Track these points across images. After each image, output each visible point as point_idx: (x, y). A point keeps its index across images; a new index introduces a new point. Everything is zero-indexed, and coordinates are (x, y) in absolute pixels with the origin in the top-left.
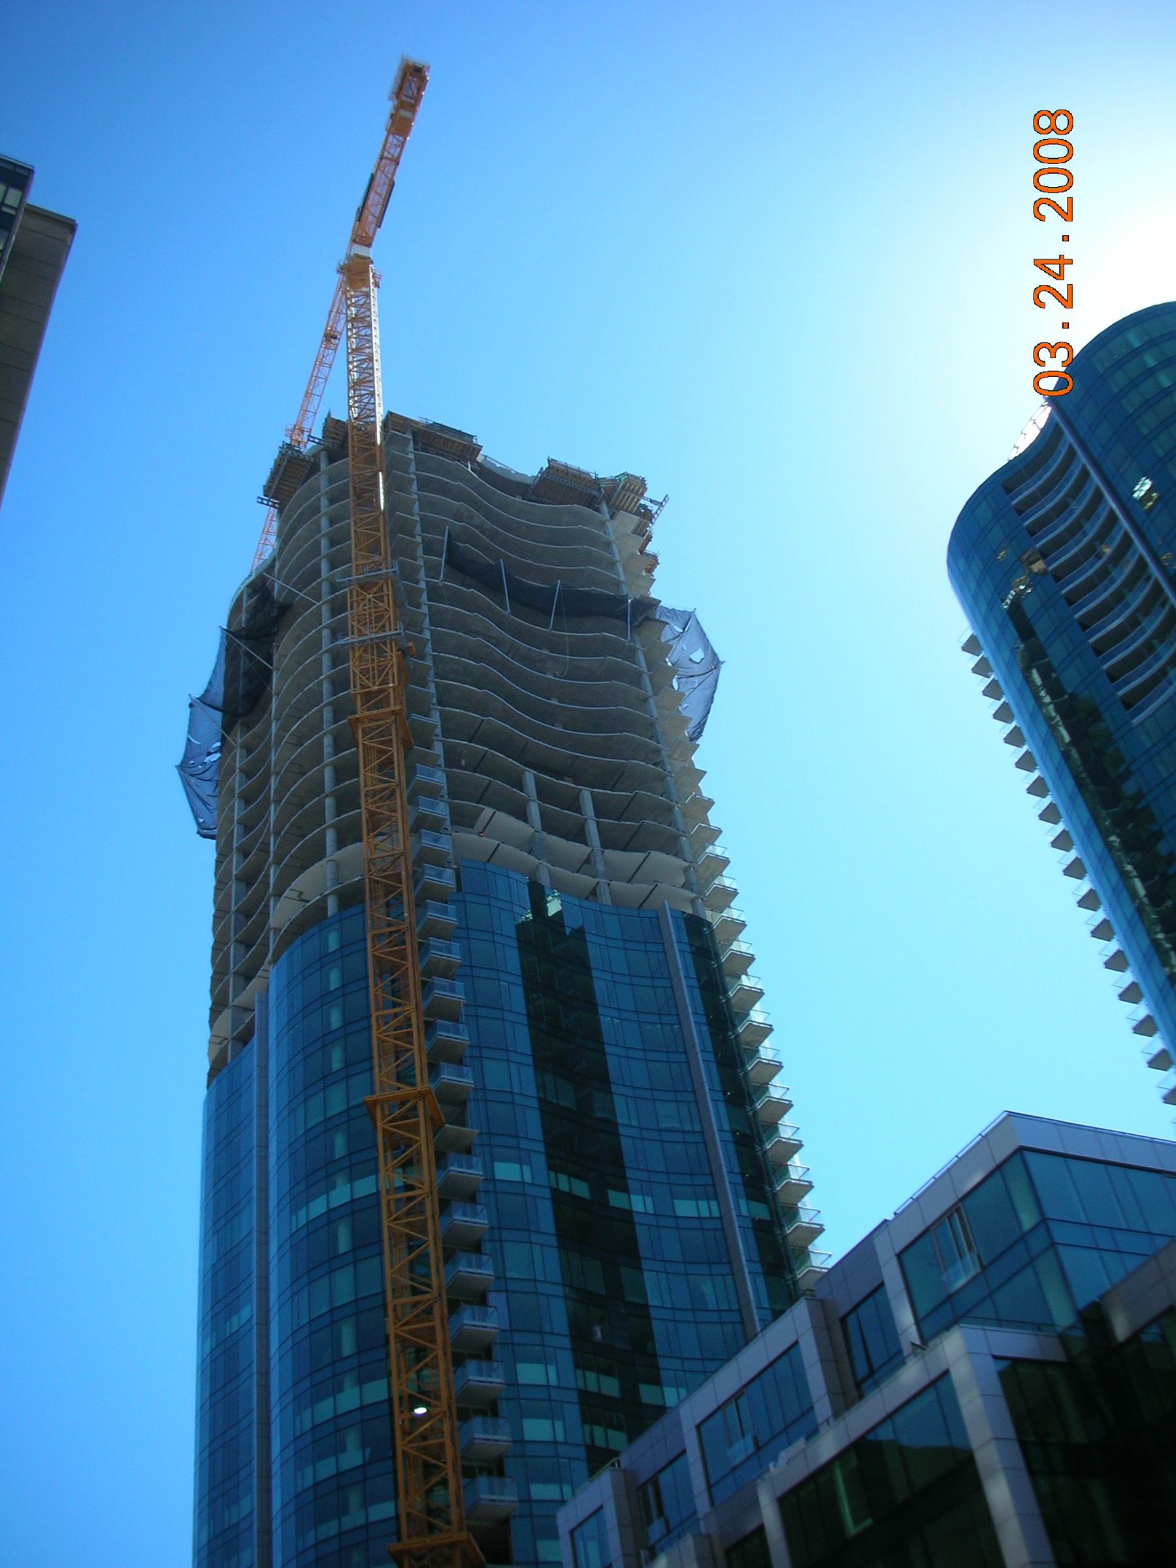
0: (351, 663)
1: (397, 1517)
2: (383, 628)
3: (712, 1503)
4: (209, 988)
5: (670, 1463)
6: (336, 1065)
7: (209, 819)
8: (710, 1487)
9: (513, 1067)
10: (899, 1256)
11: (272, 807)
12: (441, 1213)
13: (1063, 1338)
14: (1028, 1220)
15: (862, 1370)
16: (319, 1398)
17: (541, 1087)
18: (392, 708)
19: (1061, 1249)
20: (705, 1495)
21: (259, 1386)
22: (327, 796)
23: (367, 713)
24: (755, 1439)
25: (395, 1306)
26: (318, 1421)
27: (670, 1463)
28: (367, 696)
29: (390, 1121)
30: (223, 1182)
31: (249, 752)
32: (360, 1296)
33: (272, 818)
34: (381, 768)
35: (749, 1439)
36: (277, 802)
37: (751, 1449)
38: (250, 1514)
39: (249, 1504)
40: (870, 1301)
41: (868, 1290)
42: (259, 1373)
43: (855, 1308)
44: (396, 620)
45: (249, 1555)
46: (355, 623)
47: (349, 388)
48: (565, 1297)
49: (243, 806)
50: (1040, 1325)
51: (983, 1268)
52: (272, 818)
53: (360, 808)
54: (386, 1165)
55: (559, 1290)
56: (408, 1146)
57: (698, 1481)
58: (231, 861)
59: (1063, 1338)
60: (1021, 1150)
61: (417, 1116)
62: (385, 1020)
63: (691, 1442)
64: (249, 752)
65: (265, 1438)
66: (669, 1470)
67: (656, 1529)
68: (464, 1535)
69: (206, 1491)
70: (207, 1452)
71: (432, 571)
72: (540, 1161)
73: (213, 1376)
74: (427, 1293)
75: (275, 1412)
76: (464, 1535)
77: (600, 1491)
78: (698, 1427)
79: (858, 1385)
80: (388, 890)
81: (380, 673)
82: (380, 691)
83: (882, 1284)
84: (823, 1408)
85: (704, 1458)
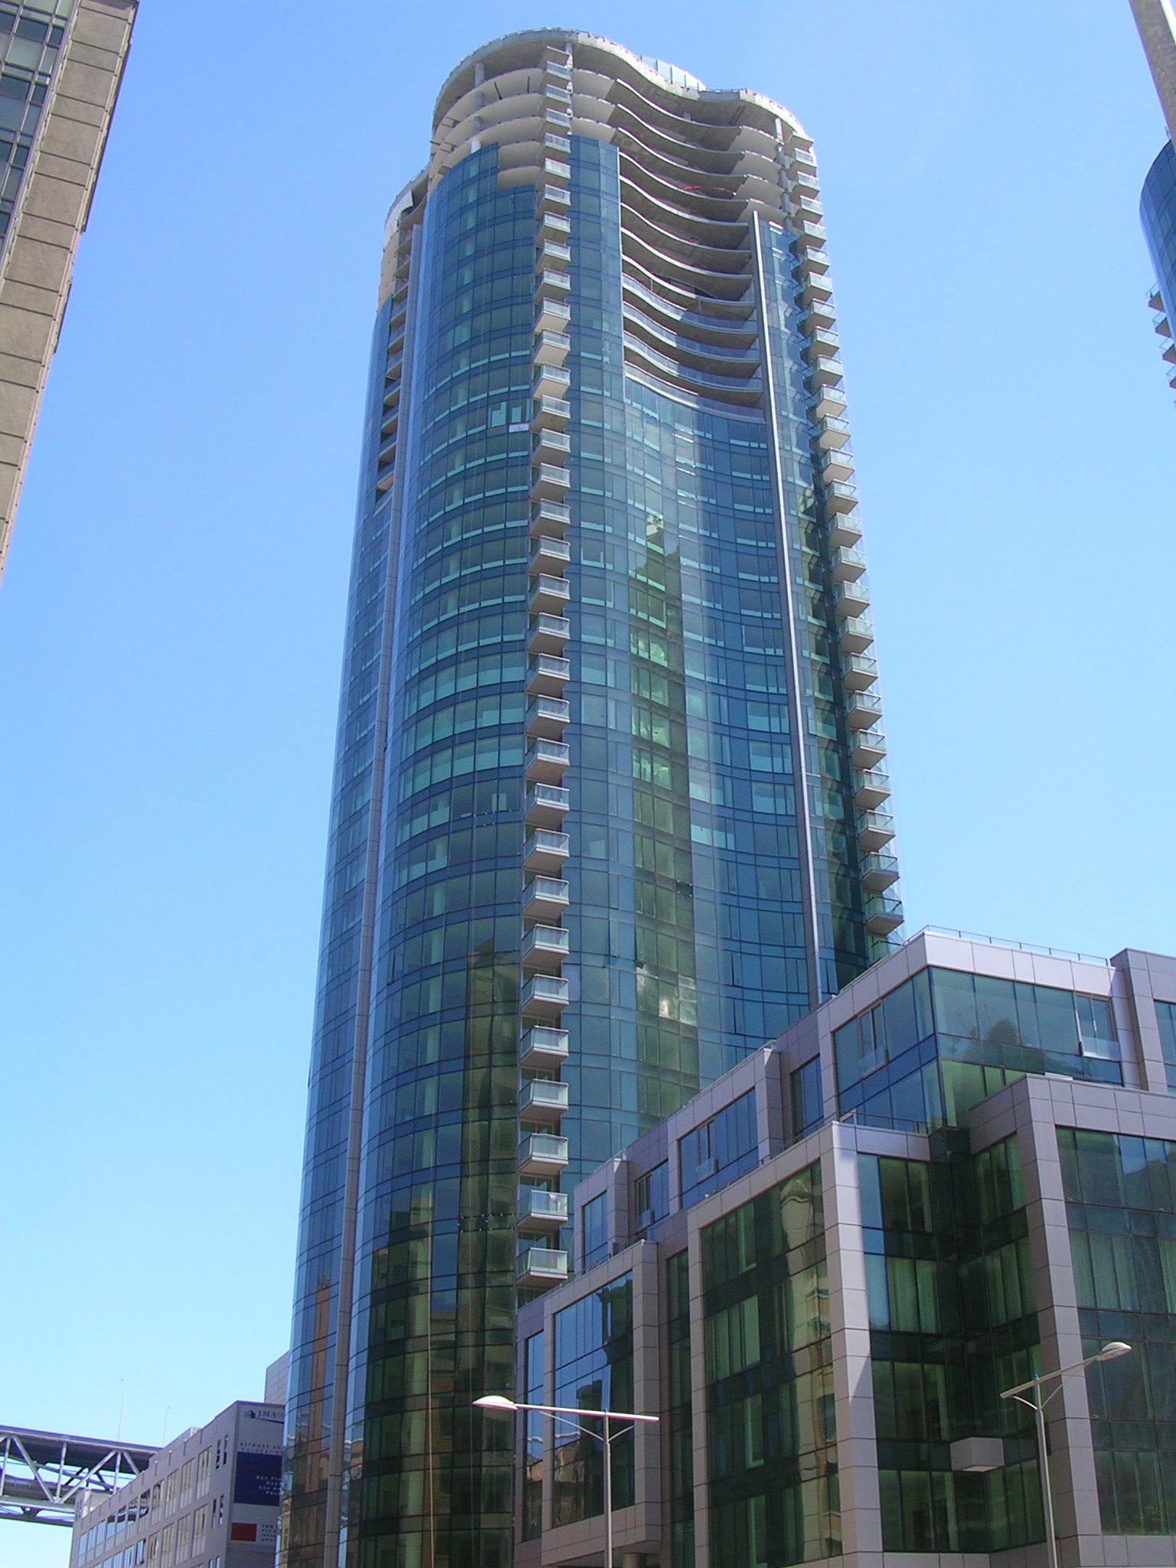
3: (681, 1207)
10: (833, 1033)
35: (712, 1159)
37: (883, 1063)
43: (802, 1067)
51: (889, 1062)
84: (764, 1149)
85: (836, 1064)
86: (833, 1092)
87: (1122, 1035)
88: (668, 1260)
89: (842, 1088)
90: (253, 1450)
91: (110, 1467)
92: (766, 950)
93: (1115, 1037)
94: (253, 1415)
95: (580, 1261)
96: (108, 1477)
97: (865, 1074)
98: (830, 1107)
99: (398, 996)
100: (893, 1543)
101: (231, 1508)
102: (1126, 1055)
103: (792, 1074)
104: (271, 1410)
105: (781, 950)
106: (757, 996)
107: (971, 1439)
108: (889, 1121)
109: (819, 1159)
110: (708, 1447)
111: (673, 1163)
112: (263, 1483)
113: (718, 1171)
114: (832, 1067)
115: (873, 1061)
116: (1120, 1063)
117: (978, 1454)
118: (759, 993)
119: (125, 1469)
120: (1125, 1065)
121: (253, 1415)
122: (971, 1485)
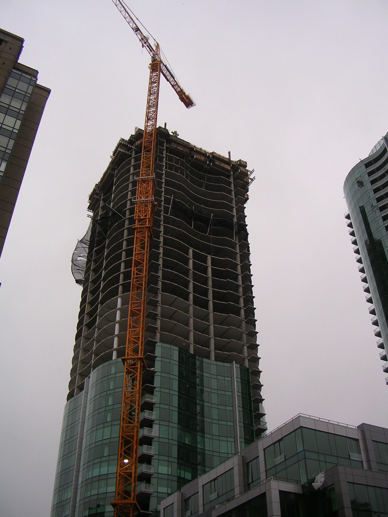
0: (137, 187)
1: (115, 492)
2: (147, 197)
4: (90, 194)
5: (195, 494)
7: (81, 277)
8: (204, 505)
10: (264, 449)
11: (106, 250)
12: (142, 396)
13: (303, 486)
14: (300, 448)
15: (250, 481)
18: (147, 225)
22: (114, 350)
23: (139, 226)
24: (218, 494)
25: (123, 426)
26: (94, 475)
27: (195, 494)
28: (140, 220)
30: (69, 427)
31: (96, 263)
33: (105, 254)
34: (147, 167)
35: (216, 493)
36: (108, 248)
37: (284, 460)
38: (69, 515)
39: (70, 494)
40: (255, 460)
41: (256, 457)
42: (83, 407)
43: (251, 461)
44: (152, 195)
45: (68, 512)
46: (137, 211)
47: (149, 84)
48: (178, 428)
49: (88, 318)
50: (297, 482)
51: (286, 460)
52: (105, 254)
53: (130, 292)
54: (121, 449)
55: (176, 426)
57: (201, 503)
58: (91, 264)
59: (303, 486)
61: (134, 432)
62: (141, 198)
64: (96, 263)
65: (78, 476)
66: (194, 496)
68: (135, 501)
69: (58, 487)
70: (59, 475)
71: (166, 212)
73: (64, 450)
74: (132, 423)
75: (83, 452)
77: (174, 498)
78: (203, 486)
80: (141, 240)
81: (146, 193)
82: (144, 219)
83: (258, 456)
84: (237, 490)
85: (203, 495)
87: (362, 452)
89: (267, 469)
93: (360, 453)
95: (264, 473)
97: (276, 464)
98: (263, 476)
102: (364, 459)
105: (167, 458)
106: (217, 438)
108: (287, 480)
109: (265, 493)
113: (218, 497)
114: (202, 496)
115: (279, 459)
116: (362, 462)
118: (218, 437)
120: (364, 462)
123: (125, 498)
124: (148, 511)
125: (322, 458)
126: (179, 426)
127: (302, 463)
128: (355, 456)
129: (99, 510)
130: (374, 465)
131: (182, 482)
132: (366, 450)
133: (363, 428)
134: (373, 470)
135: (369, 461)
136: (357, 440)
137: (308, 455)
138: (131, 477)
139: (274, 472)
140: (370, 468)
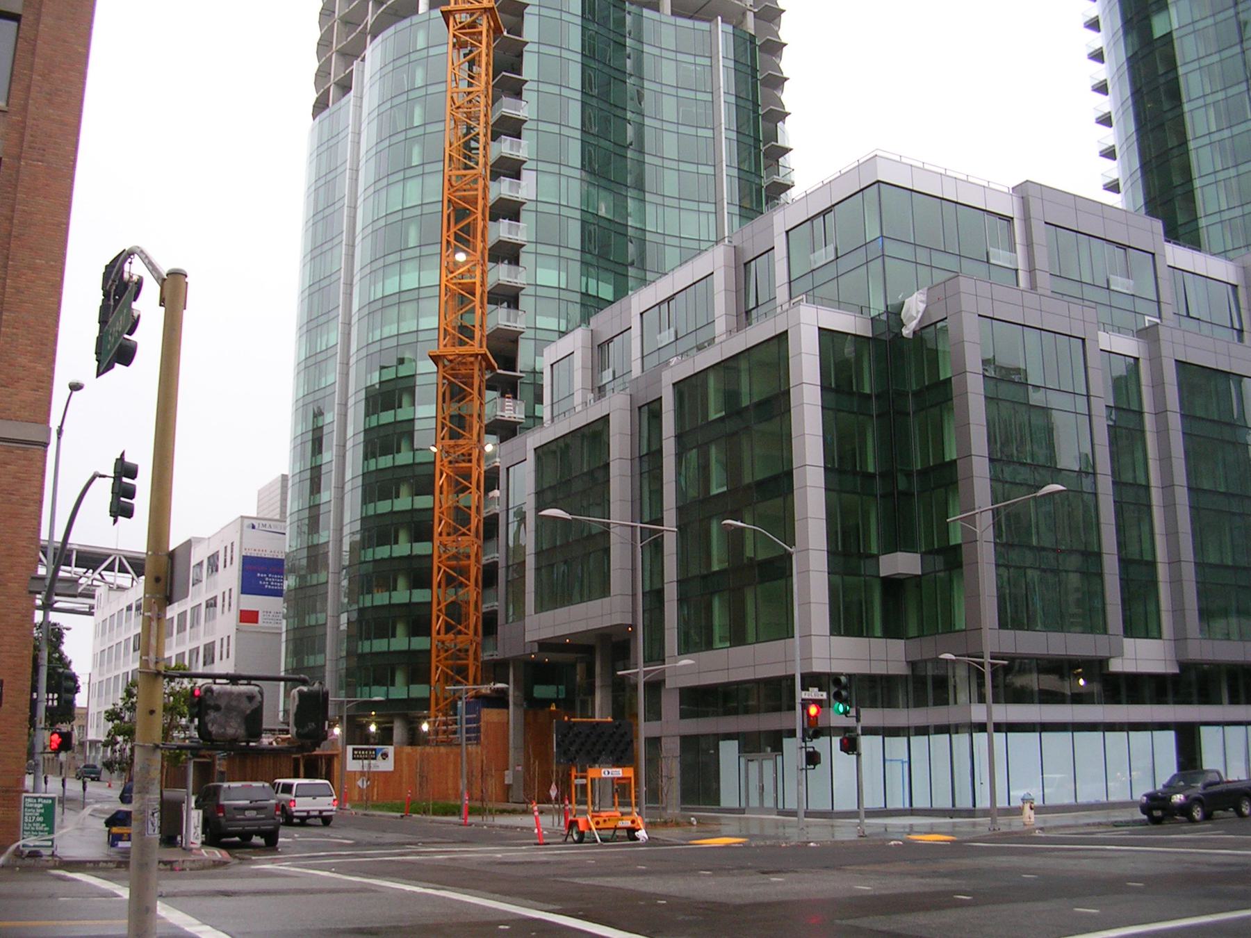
6: (416, 160)
9: (563, 180)
10: (787, 232)
14: (873, 233)
15: (752, 304)
16: (380, 544)
17: (586, 198)
19: (887, 259)
20: (639, 361)
21: (349, 216)
29: (463, 28)
32: (426, 201)
35: (672, 330)
37: (833, 257)
54: (448, 230)
56: (469, 215)
60: (878, 181)
63: (636, 323)
67: (607, 376)
68: (485, 350)
72: (576, 267)
74: (473, 168)
76: (485, 350)
77: (576, 342)
79: (748, 313)
84: (720, 326)
86: (639, 355)
87: (1019, 248)
88: (640, 408)
90: (254, 554)
91: (110, 568)
92: (684, 204)
94: (253, 527)
96: (109, 576)
99: (384, 192)
100: (836, 630)
101: (238, 599)
102: (1022, 266)
103: (745, 264)
104: (268, 523)
107: (899, 553)
108: (839, 304)
110: (536, 531)
111: (636, 331)
112: (263, 579)
116: (1017, 270)
117: (903, 563)
119: (123, 570)
121: (253, 527)
122: (894, 586)
123: (462, 343)
124: (515, 371)
125: (923, 256)
126: (884, 317)
127: (876, 266)
128: (1000, 257)
129: (404, 371)
130: (1043, 280)
131: (591, 305)
132: (1029, 245)
133: (1025, 192)
134: (1040, 291)
135: (1032, 271)
136: (1010, 220)
137: (891, 248)
138: (473, 294)
139: (807, 286)
140: (1033, 286)
